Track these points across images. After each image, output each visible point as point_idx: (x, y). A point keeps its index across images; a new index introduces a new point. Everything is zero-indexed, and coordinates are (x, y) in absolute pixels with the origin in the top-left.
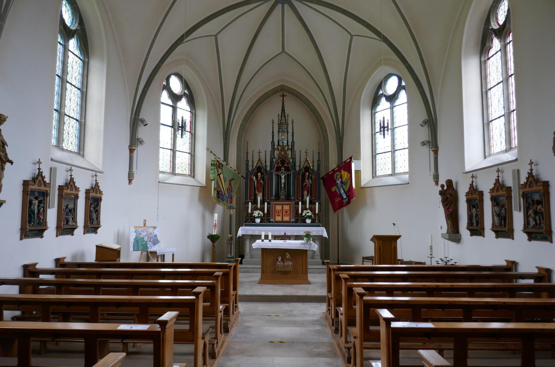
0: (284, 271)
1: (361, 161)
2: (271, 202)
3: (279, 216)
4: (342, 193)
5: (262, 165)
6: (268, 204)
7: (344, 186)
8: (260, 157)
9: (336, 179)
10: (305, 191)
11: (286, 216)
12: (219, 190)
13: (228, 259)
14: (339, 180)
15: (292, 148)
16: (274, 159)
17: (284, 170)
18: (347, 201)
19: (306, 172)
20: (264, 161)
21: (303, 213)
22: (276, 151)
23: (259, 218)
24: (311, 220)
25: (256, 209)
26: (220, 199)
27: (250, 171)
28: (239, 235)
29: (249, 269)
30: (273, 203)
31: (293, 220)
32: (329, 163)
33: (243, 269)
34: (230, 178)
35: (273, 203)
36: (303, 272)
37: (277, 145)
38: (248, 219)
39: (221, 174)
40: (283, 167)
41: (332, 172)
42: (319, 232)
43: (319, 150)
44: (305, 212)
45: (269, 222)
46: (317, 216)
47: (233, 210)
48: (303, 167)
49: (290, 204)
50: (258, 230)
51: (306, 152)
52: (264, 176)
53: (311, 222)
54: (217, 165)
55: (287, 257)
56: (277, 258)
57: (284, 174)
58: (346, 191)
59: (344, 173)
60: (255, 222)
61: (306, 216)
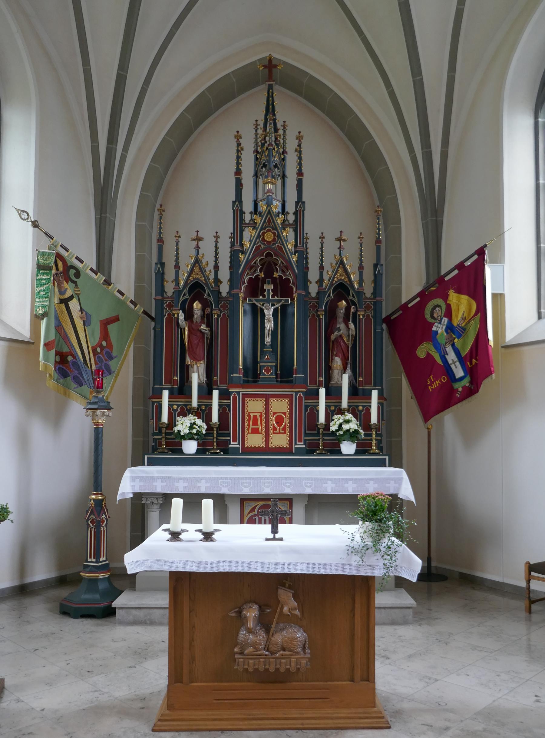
0: (272, 670)
1: (507, 266)
2: (231, 390)
3: (255, 431)
4: (450, 362)
5: (207, 278)
6: (221, 397)
7: (456, 340)
8: (198, 253)
9: (430, 320)
10: (336, 355)
11: (279, 433)
12: (66, 349)
13: (90, 572)
14: (440, 323)
15: (296, 221)
16: (242, 253)
17: (271, 293)
18: (468, 385)
19: (340, 301)
20: (212, 264)
21: (331, 424)
22: (246, 229)
23: (192, 439)
24: (355, 444)
25: (186, 411)
26: (69, 379)
27: (168, 297)
28: (124, 494)
29: (155, 610)
30: (238, 393)
31: (301, 445)
32: (401, 283)
33: (134, 612)
34: (105, 315)
35: (238, 393)
36: (352, 668)
37: (251, 213)
38: (160, 444)
39: (71, 298)
40: (269, 283)
41: (418, 299)
42: (388, 485)
43: (379, 234)
44: (337, 419)
45: (226, 451)
46: (374, 433)
47: (103, 415)
48: (332, 284)
49: (290, 397)
50: (185, 479)
51: (339, 239)
52: (212, 311)
53: (357, 452)
54: (57, 269)
55: (286, 609)
56: (240, 612)
57: (273, 305)
58: (463, 355)
59: (459, 300)
60: (181, 452)
61: (341, 432)
